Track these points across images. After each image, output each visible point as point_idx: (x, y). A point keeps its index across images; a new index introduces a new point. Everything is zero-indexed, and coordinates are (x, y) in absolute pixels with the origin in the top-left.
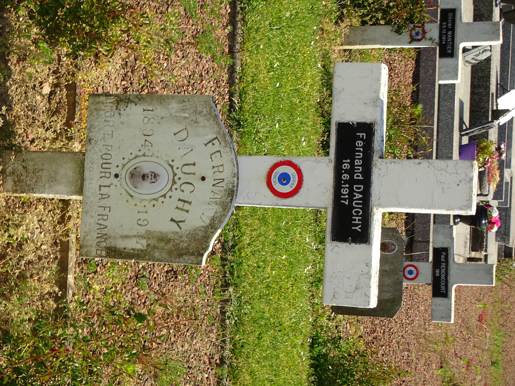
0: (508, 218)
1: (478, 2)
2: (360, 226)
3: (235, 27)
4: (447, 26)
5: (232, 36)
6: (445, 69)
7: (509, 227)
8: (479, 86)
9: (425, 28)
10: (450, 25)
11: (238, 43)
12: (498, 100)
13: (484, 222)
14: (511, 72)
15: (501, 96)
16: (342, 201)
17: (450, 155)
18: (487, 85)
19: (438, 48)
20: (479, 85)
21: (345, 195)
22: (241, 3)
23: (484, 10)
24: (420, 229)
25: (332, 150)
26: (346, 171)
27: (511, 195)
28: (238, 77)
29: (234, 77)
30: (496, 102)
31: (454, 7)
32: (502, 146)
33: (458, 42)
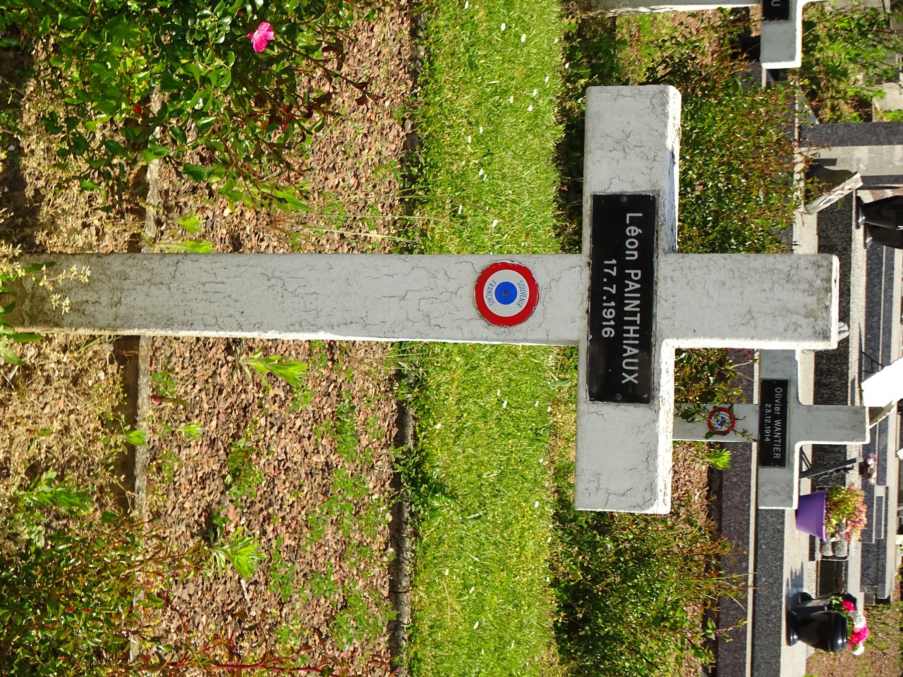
0: (881, 551)
1: (826, 224)
2: (636, 375)
3: (399, 550)
4: (773, 411)
5: (395, 567)
6: (770, 487)
7: (884, 567)
8: (829, 373)
9: (735, 413)
10: (777, 409)
11: (406, 575)
12: (863, 384)
13: (840, 642)
14: (884, 315)
15: (867, 377)
16: (606, 270)
17: (779, 527)
18: (842, 370)
19: (755, 445)
20: (828, 370)
21: (609, 320)
22: (411, 505)
23: (836, 237)
24: (728, 661)
25: (587, 245)
26: (611, 281)
27: (886, 510)
28: (406, 637)
29: (399, 636)
30: (860, 386)
31: (785, 378)
32: (871, 462)
33: (792, 439)
